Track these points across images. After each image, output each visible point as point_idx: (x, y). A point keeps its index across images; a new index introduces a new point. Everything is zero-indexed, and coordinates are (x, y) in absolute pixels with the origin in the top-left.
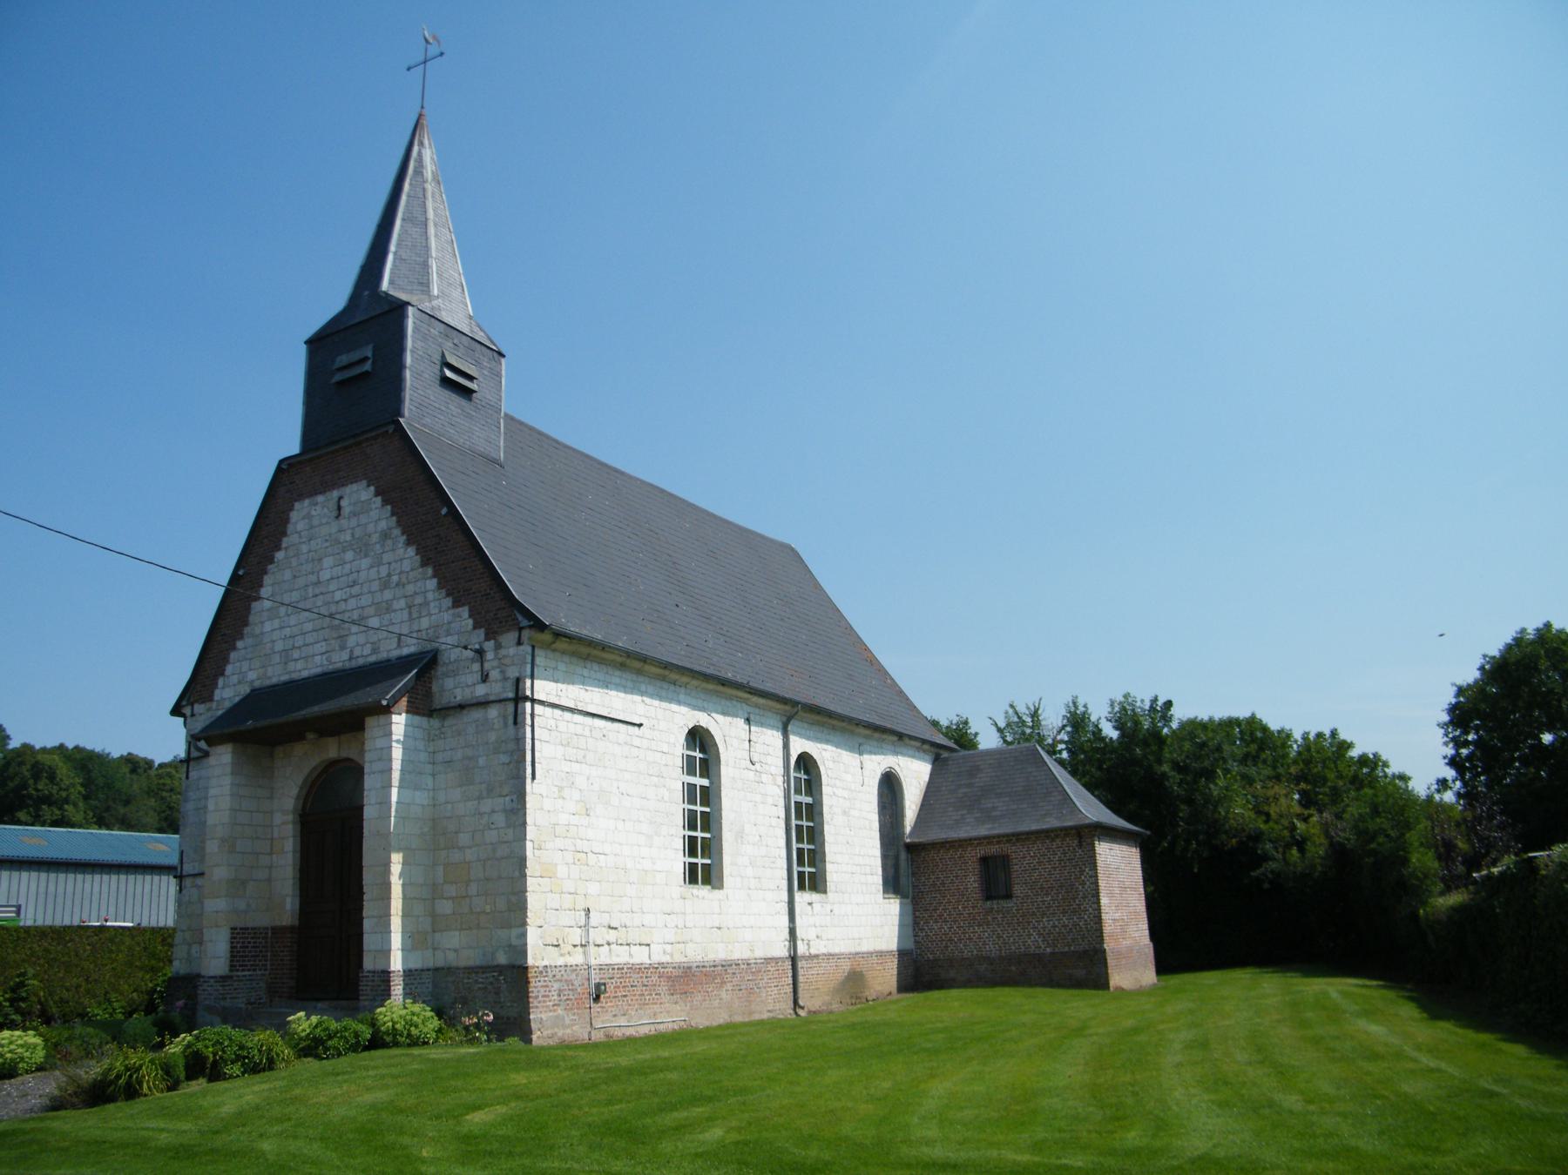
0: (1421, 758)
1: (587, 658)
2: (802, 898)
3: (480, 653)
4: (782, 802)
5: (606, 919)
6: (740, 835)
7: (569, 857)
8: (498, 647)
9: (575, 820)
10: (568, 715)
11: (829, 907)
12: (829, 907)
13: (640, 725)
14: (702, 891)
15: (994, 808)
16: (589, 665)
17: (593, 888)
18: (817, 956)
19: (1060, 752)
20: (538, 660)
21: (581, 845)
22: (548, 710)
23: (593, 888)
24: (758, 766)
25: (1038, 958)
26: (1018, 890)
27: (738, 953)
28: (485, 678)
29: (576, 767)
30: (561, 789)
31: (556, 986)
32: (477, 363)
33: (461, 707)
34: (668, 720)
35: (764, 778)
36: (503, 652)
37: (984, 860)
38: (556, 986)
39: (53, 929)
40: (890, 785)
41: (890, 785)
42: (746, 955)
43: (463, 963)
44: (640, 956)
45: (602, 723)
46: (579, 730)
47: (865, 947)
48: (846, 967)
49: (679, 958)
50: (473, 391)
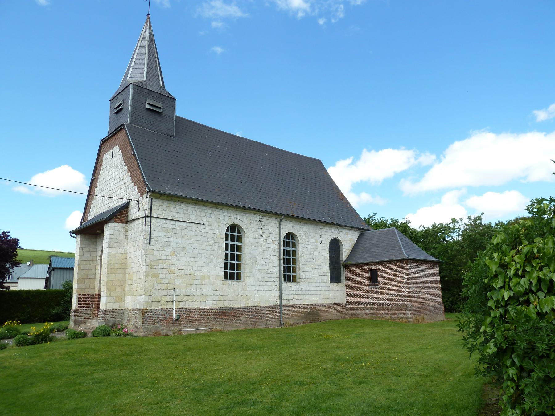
0: (527, 214)
1: (178, 201)
2: (285, 285)
3: (138, 201)
4: (278, 250)
5: (183, 292)
6: (255, 262)
7: (166, 271)
8: (143, 199)
9: (170, 258)
10: (168, 222)
11: (300, 288)
12: (300, 288)
13: (204, 224)
14: (234, 283)
15: (375, 252)
16: (179, 204)
17: (177, 282)
18: (293, 305)
19: (531, 242)
20: (154, 203)
21: (171, 267)
22: (158, 220)
23: (177, 282)
24: (265, 238)
25: (387, 308)
26: (380, 282)
27: (251, 304)
28: (139, 210)
29: (170, 240)
30: (163, 247)
31: (156, 316)
32: (163, 103)
33: (134, 220)
34: (218, 222)
35: (268, 242)
36: (144, 201)
37: (370, 271)
38: (156, 316)
39: (443, 289)
40: (335, 245)
41: (335, 245)
42: (255, 304)
43: (130, 308)
44: (204, 306)
45: (185, 224)
46: (173, 226)
47: (319, 302)
48: (309, 309)
49: (220, 306)
50: (161, 113)
